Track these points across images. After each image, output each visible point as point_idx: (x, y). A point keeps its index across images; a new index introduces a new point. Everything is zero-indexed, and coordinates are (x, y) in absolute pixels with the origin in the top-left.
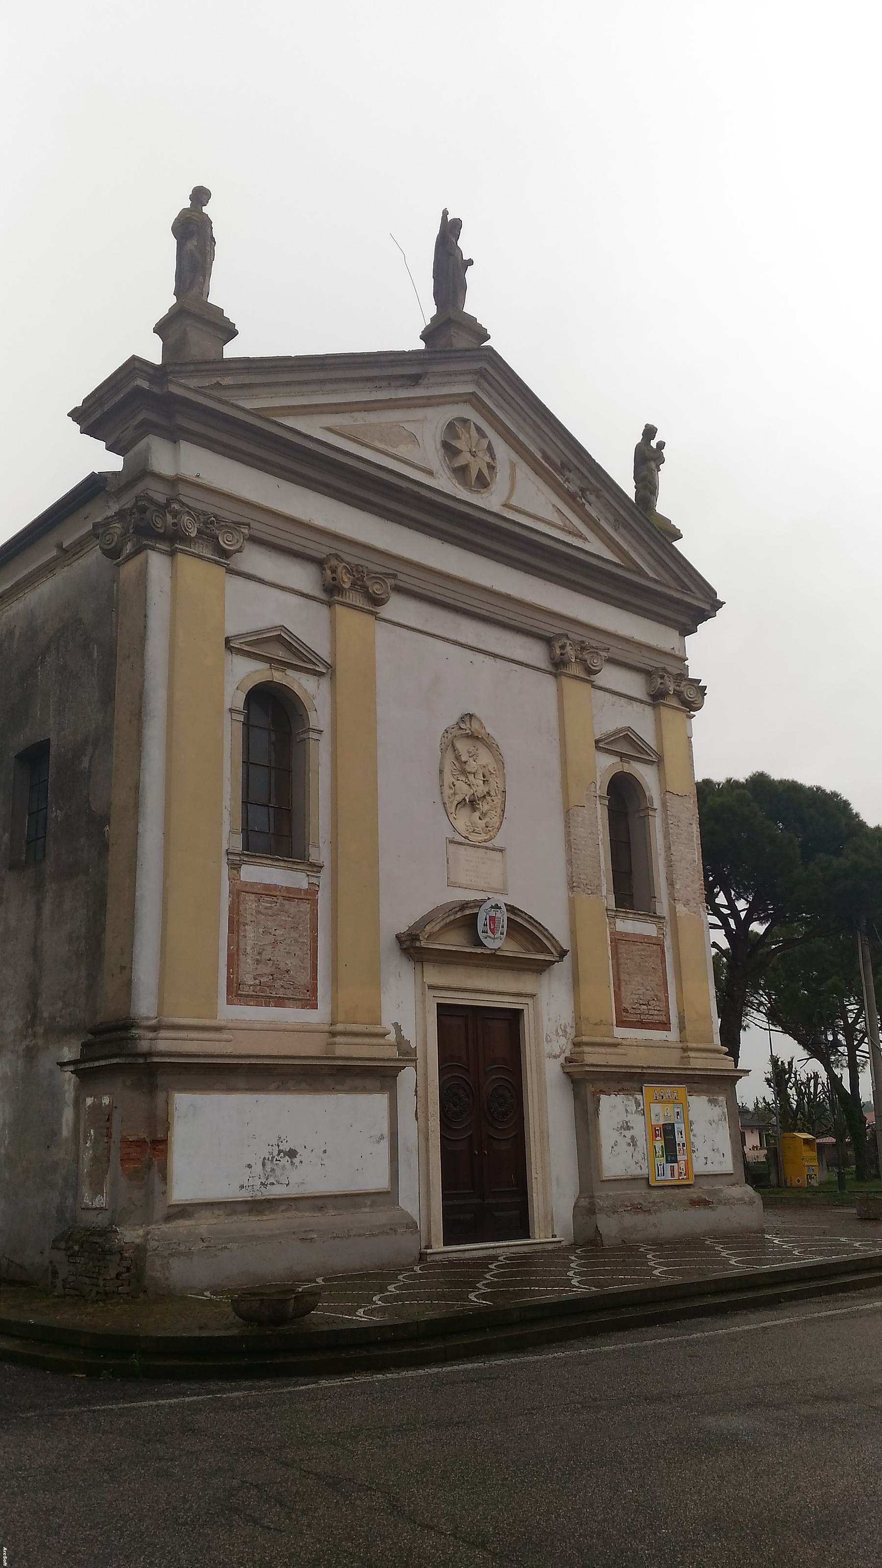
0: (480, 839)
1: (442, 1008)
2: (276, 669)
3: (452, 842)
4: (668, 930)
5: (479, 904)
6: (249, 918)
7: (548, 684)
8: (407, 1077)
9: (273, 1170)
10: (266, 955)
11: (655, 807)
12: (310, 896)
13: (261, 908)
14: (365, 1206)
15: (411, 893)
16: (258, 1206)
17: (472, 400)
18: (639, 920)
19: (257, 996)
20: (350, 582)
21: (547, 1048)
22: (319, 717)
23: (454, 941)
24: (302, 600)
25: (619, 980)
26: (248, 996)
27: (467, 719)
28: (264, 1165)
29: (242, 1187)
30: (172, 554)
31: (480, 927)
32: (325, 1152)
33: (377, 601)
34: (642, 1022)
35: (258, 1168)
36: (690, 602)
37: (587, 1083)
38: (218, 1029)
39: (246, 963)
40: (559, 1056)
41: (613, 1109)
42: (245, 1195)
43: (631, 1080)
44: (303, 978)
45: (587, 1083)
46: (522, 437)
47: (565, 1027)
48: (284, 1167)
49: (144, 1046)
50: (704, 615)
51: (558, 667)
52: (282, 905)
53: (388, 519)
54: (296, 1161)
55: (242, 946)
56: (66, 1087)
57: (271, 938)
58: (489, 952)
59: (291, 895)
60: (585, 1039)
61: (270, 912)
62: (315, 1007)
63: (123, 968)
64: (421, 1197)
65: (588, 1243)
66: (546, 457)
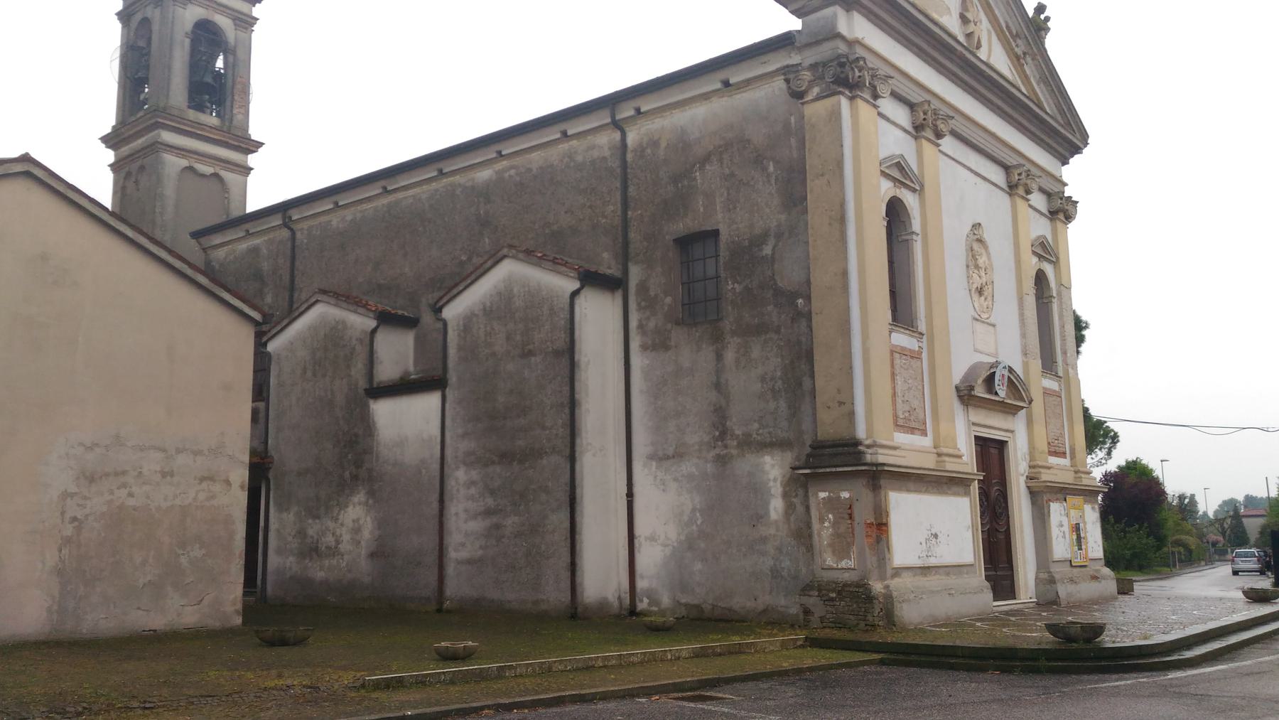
4: (924, 345)
15: (963, 355)
30: (852, 99)
31: (997, 382)
33: (939, 135)
36: (1066, 136)
37: (1041, 494)
38: (895, 448)
41: (1057, 512)
42: (919, 563)
43: (1063, 492)
45: (1041, 494)
46: (997, 12)
49: (869, 458)
50: (1077, 150)
51: (1012, 188)
53: (941, 73)
56: (771, 484)
60: (945, 450)
63: (841, 403)
65: (1048, 602)
66: (1007, 27)
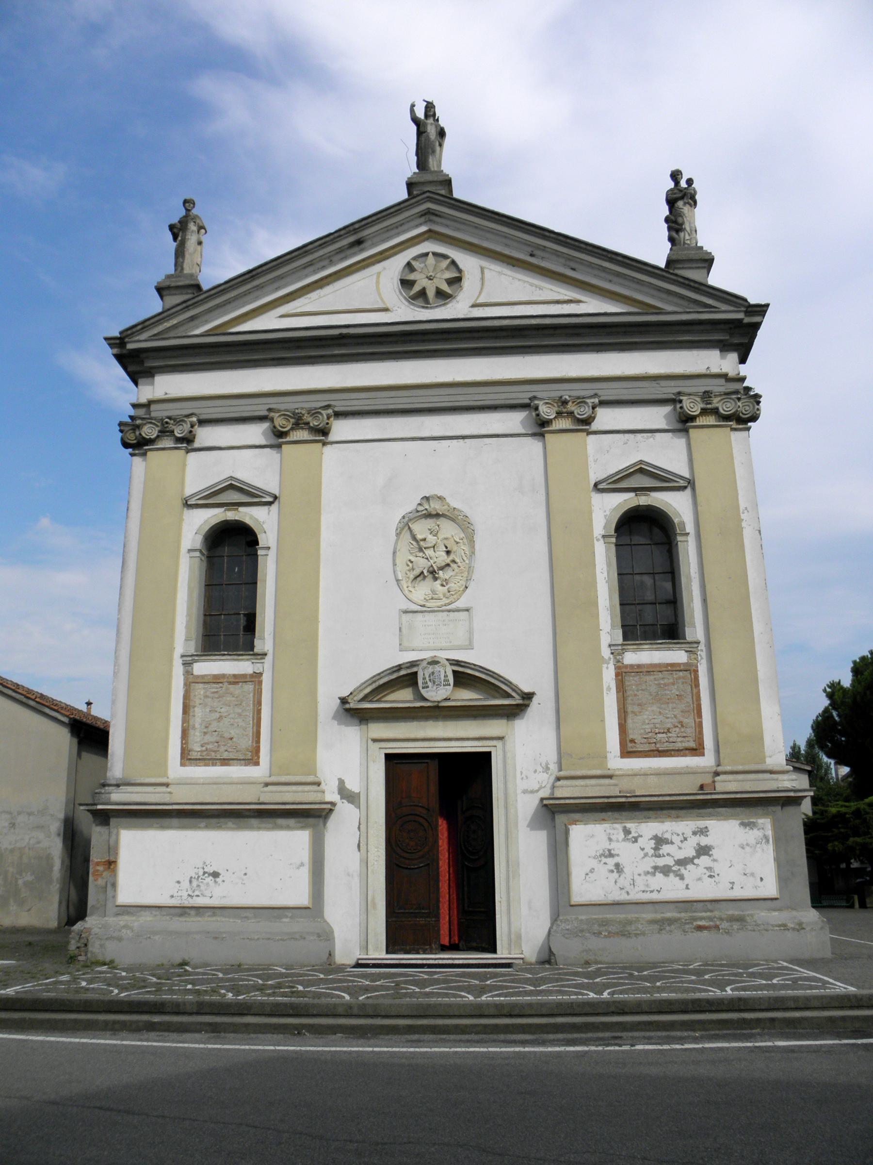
0: (443, 603)
1: (389, 757)
2: (229, 510)
3: (406, 612)
4: (702, 653)
5: (413, 664)
6: (198, 702)
7: (535, 445)
8: (346, 817)
9: (198, 886)
10: (211, 729)
11: (687, 531)
12: (691, 670)
13: (208, 694)
14: (287, 917)
16: (183, 911)
17: (431, 235)
18: (657, 649)
19: (204, 759)
20: (301, 424)
21: (521, 785)
22: (268, 538)
23: (403, 697)
24: (257, 450)
25: (625, 712)
26: (196, 759)
27: (424, 502)
28: (191, 882)
29: (172, 896)
32: (245, 874)
34: (658, 751)
35: (186, 884)
39: (194, 735)
40: (537, 791)
44: (246, 742)
47: (547, 764)
48: (208, 884)
51: (541, 427)
52: (227, 689)
54: (219, 880)
55: (191, 723)
57: (216, 715)
58: (429, 704)
59: (237, 680)
61: (216, 695)
62: (257, 763)
64: (354, 915)
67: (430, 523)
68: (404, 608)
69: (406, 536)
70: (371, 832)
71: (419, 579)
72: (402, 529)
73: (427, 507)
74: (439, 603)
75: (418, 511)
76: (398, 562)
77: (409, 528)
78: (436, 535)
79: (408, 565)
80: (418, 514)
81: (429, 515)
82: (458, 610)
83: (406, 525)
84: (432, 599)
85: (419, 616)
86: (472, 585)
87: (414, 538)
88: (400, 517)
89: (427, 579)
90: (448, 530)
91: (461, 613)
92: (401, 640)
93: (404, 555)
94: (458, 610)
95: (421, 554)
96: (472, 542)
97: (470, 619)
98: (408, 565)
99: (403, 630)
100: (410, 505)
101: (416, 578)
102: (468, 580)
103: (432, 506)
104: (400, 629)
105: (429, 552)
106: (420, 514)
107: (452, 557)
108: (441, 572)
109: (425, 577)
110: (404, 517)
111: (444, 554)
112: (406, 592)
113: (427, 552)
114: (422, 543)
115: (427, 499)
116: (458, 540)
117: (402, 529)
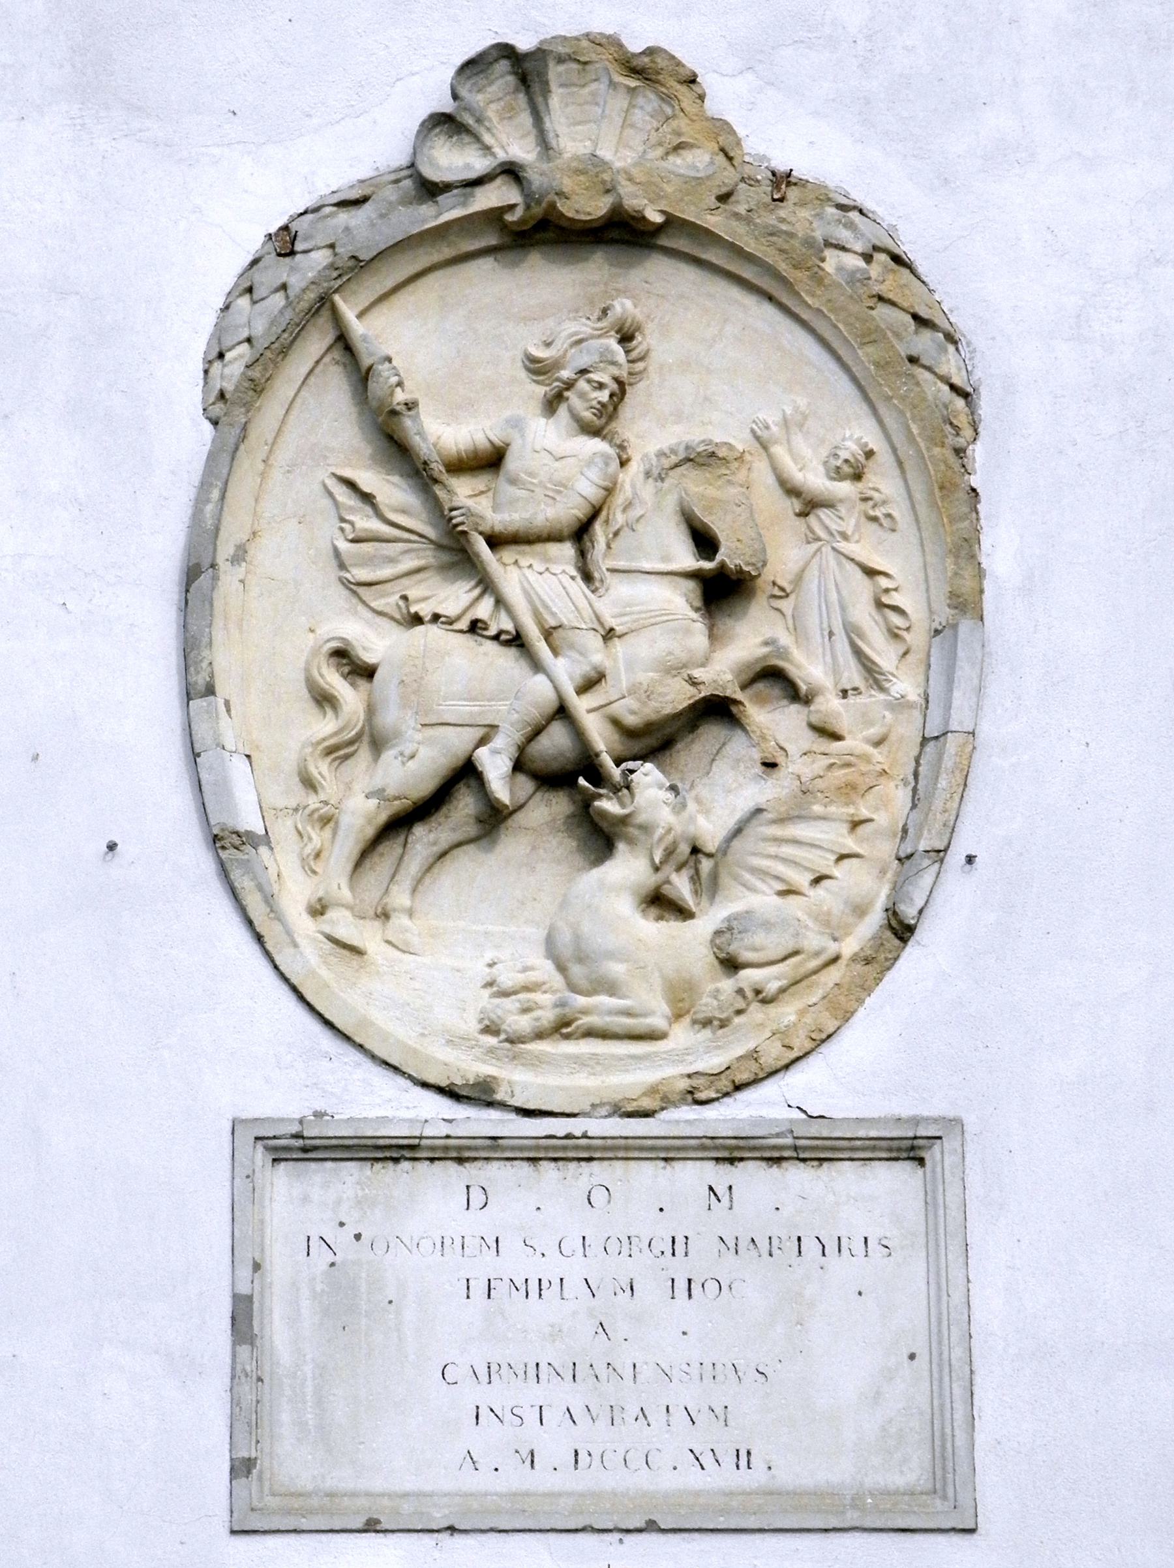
3: (301, 1148)
27: (495, 95)
67: (548, 302)
68: (284, 1105)
69: (317, 424)
70: (825, 1134)
71: (425, 839)
72: (276, 351)
73: (521, 150)
74: (632, 1073)
75: (430, 190)
76: (226, 659)
77: (343, 342)
78: (600, 424)
79: (324, 700)
80: (430, 216)
81: (540, 231)
82: (812, 1148)
83: (308, 306)
84: (562, 1028)
85: (435, 1193)
86: (953, 912)
87: (392, 440)
88: (252, 239)
89: (512, 845)
90: (724, 375)
91: (844, 1179)
92: (248, 1415)
93: (292, 601)
94: (812, 1148)
95: (454, 597)
96: (954, 504)
97: (943, 1235)
98: (324, 700)
99: (278, 1329)
100: (358, 129)
101: (400, 823)
102: (920, 855)
103: (572, 142)
104: (243, 1319)
105: (538, 583)
106: (451, 210)
107: (750, 636)
108: (647, 775)
109: (494, 819)
110: (286, 243)
111: (679, 601)
112: (308, 958)
113: (515, 575)
114: (464, 492)
115: (522, 70)
116: (815, 480)
117: (276, 351)
